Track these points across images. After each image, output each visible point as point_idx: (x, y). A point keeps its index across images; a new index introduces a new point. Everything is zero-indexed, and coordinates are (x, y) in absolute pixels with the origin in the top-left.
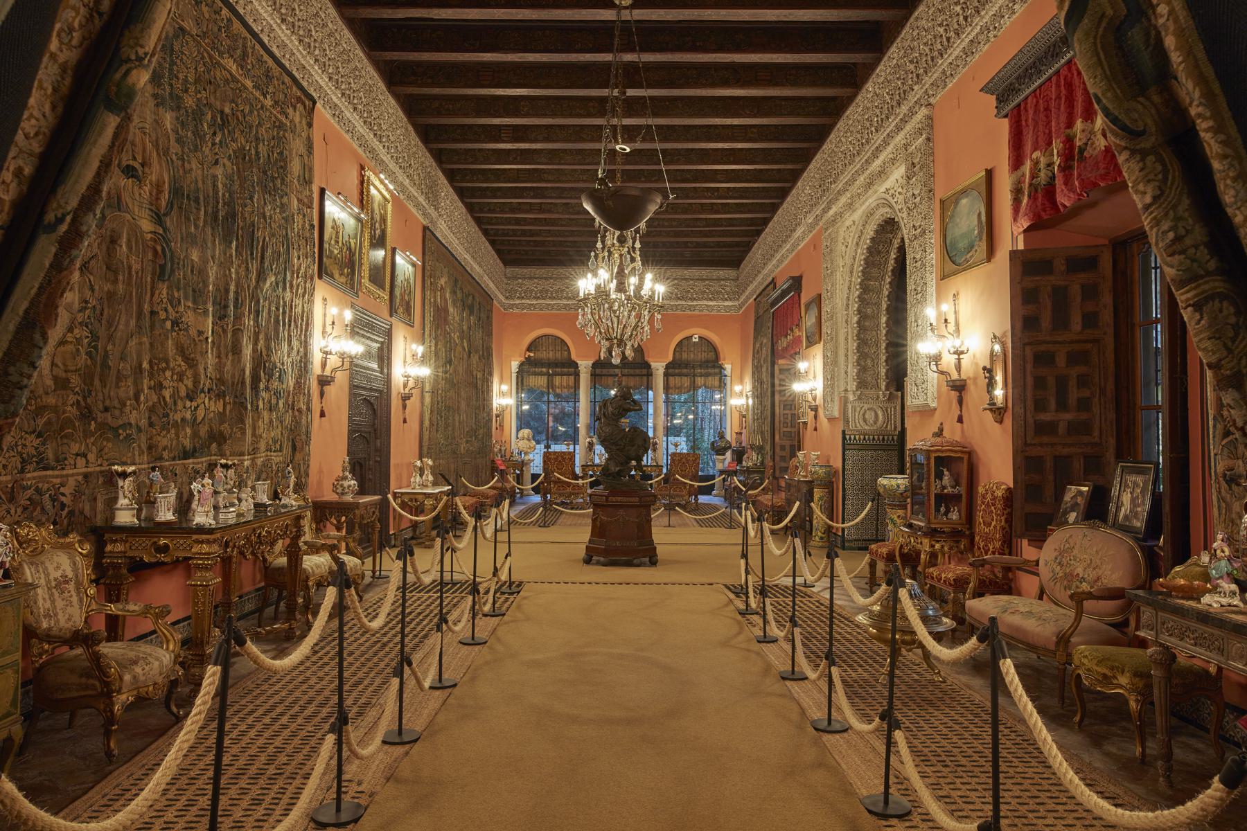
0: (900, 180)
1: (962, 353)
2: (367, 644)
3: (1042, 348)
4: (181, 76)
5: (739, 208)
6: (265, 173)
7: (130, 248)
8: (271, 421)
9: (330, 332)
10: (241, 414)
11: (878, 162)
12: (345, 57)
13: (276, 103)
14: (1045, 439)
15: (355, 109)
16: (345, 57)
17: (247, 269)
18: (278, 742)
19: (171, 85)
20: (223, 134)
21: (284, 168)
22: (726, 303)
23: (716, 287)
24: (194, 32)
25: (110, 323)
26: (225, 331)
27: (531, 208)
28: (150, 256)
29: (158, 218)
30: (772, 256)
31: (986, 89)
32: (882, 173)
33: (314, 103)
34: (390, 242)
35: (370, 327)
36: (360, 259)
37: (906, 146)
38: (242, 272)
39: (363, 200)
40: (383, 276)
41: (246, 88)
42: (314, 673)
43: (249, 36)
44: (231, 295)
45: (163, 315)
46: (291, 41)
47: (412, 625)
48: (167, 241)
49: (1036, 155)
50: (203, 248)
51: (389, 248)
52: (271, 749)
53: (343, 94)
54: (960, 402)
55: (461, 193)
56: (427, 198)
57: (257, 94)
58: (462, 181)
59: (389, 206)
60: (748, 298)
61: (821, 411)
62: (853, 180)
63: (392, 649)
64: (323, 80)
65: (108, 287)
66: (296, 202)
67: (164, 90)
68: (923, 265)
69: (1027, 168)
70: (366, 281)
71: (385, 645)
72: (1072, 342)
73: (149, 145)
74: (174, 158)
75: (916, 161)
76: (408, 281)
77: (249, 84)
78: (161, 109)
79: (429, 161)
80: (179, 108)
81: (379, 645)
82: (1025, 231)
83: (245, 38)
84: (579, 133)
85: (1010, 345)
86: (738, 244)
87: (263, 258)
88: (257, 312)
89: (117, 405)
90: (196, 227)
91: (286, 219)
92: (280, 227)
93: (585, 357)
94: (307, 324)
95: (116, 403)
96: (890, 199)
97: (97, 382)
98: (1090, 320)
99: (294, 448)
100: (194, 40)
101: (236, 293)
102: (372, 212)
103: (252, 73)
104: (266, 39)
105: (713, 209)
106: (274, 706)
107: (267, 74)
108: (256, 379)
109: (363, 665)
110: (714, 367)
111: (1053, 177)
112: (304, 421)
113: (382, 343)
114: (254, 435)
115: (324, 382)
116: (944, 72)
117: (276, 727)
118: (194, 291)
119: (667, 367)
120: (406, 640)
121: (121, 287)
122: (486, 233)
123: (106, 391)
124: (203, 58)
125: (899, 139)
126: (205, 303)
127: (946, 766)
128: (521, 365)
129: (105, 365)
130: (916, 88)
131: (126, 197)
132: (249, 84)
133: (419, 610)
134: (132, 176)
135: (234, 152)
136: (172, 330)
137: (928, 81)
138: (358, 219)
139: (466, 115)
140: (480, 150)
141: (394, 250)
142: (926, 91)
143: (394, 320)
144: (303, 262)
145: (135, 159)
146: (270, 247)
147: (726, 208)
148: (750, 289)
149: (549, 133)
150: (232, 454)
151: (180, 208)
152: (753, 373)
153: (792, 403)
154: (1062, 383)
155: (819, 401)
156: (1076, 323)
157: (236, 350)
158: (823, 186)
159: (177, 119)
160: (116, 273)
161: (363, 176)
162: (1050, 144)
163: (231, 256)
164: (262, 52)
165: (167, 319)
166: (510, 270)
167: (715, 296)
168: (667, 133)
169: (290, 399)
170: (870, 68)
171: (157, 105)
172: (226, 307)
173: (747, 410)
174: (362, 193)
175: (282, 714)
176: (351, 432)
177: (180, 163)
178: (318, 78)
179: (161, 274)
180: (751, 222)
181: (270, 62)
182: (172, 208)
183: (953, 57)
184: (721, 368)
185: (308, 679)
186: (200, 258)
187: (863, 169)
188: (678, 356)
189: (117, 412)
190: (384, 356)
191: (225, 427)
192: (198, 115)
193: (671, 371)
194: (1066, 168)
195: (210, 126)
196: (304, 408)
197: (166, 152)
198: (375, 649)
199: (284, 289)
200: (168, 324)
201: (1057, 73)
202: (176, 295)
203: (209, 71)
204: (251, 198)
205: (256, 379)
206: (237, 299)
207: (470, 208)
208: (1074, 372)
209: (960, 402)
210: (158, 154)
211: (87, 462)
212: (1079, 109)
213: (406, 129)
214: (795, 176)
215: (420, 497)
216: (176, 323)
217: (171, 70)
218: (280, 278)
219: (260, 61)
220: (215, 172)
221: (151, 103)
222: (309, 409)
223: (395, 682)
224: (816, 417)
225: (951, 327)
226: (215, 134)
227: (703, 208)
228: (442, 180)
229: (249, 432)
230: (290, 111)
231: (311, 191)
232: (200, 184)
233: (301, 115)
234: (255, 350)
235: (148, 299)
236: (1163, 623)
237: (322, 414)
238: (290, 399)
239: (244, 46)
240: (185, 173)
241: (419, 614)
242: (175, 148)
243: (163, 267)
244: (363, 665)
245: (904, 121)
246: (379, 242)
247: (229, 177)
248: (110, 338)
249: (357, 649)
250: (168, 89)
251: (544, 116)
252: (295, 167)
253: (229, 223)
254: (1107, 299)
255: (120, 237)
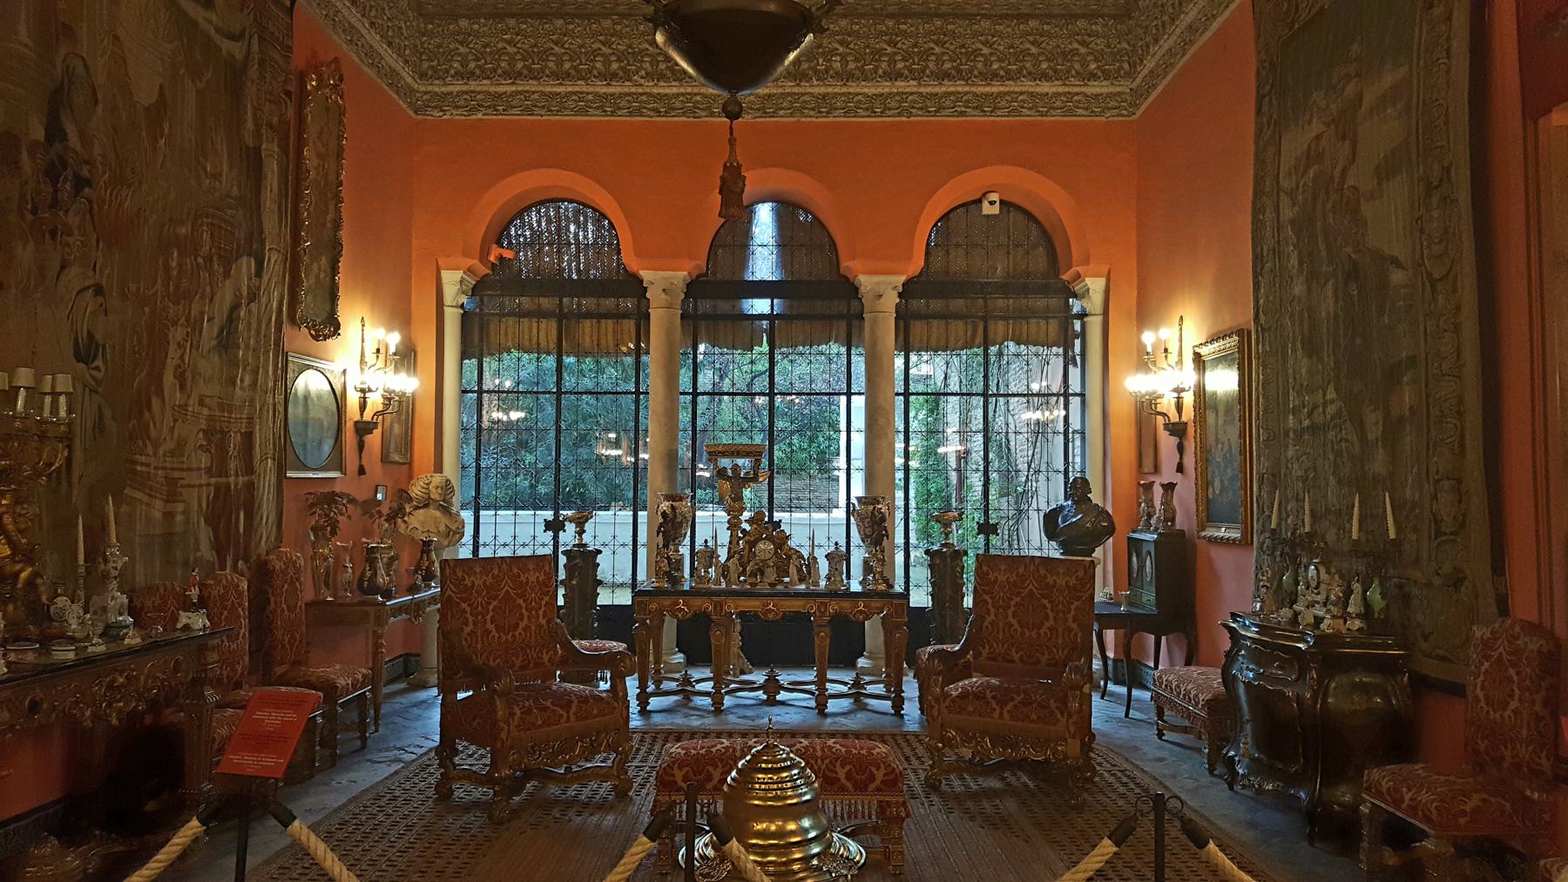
22: (1095, 88)
93: (660, 258)
110: (1044, 290)
115: (363, 429)
119: (907, 292)
188: (938, 263)
193: (919, 304)
225: (1173, 358)
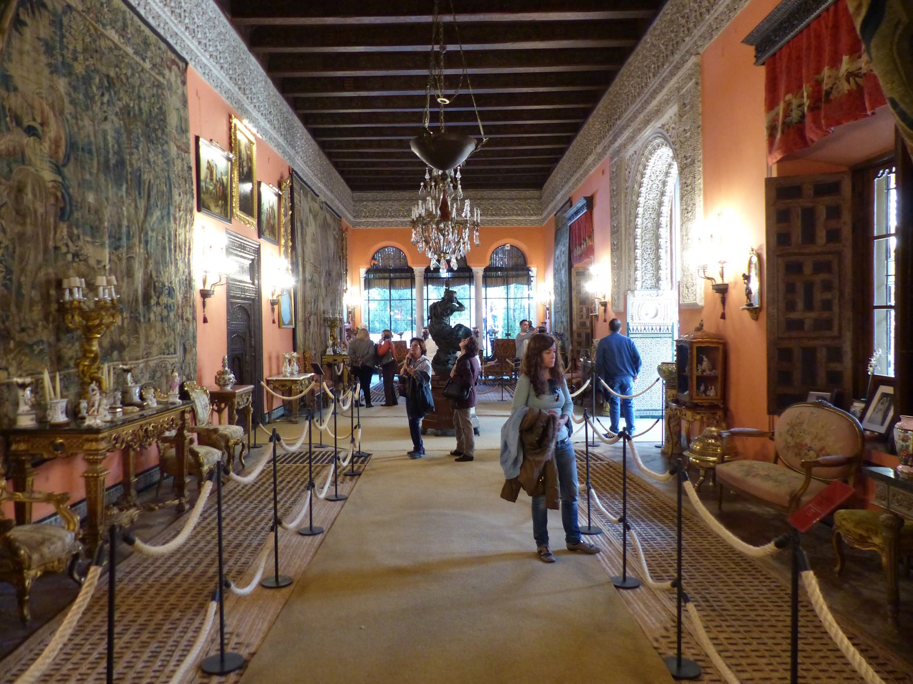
0: (673, 117)
1: (724, 262)
2: (247, 511)
3: (793, 258)
4: (71, 47)
5: (540, 141)
6: (147, 125)
7: (35, 195)
8: (163, 330)
9: (210, 255)
10: (136, 326)
11: (655, 103)
12: (211, 24)
13: (154, 65)
14: (794, 334)
15: (222, 67)
16: (211, 24)
17: (136, 207)
18: (173, 599)
19: (63, 55)
20: (110, 95)
21: (164, 120)
23: (523, 204)
24: (80, 8)
25: (22, 259)
26: (120, 259)
27: (370, 144)
28: (52, 201)
29: (58, 169)
30: (569, 179)
31: (747, 41)
32: (658, 112)
33: (187, 64)
34: (257, 176)
35: (242, 247)
36: (231, 192)
37: (679, 89)
38: (132, 211)
39: (232, 144)
40: (250, 205)
41: (127, 54)
42: (204, 537)
43: (128, 10)
44: (124, 230)
45: (64, 249)
46: (164, 12)
47: (283, 493)
48: (66, 188)
49: (789, 97)
50: (97, 191)
51: (255, 182)
52: (167, 606)
53: (211, 56)
54: (724, 301)
55: (315, 133)
56: (286, 139)
57: (138, 59)
58: (315, 123)
59: (254, 148)
60: (549, 214)
61: (609, 306)
62: (635, 116)
63: (267, 514)
64: (193, 45)
65: (18, 229)
66: (175, 148)
67: (56, 59)
68: (693, 189)
69: (781, 107)
70: (237, 211)
71: (261, 510)
72: (817, 254)
73: (47, 108)
74: (69, 117)
75: (687, 102)
76: (272, 208)
77: (130, 50)
78: (55, 77)
79: (286, 107)
80: (70, 74)
81: (257, 510)
82: (778, 162)
83: (124, 12)
84: (410, 83)
85: (765, 257)
86: (541, 170)
87: (149, 196)
88: (147, 242)
89: (32, 327)
90: (91, 174)
91: (167, 163)
92: (162, 170)
94: (190, 249)
95: (30, 325)
96: (665, 133)
97: (13, 308)
98: (834, 236)
99: (185, 350)
100: (81, 15)
101: (128, 227)
102: (240, 152)
103: (132, 41)
104: (142, 12)
105: (520, 142)
106: (170, 567)
107: (146, 43)
108: (147, 298)
109: (243, 529)
110: (523, 269)
111: (803, 116)
112: (191, 328)
113: (253, 260)
114: (147, 342)
116: (710, 26)
117: (172, 585)
118: (92, 228)
120: (279, 506)
121: (29, 229)
122: (336, 165)
123: (22, 315)
124: (89, 30)
125: (673, 83)
126: (102, 237)
127: (714, 610)
128: (368, 272)
129: (19, 294)
130: (687, 39)
131: (28, 152)
132: (130, 50)
133: (288, 479)
134: (34, 135)
135: (121, 109)
136: (73, 261)
137: (697, 33)
138: (229, 159)
139: (315, 70)
140: (327, 98)
141: (259, 183)
142: (695, 42)
143: (262, 241)
144: (183, 198)
145: (34, 120)
146: (155, 187)
147: (529, 141)
148: (551, 206)
149: (384, 83)
150: (130, 359)
151: (76, 159)
152: (555, 275)
153: (586, 303)
154: (809, 288)
155: (608, 299)
156: (821, 236)
157: (130, 274)
158: (610, 121)
159: (69, 84)
160: (24, 216)
161: (230, 123)
162: (801, 87)
163: (122, 197)
164: (140, 23)
165: (68, 252)
166: (357, 194)
167: (523, 212)
168: (479, 80)
169: (180, 311)
170: (648, 22)
171: (52, 73)
172: (120, 239)
173: (550, 304)
174: (230, 137)
175: (177, 574)
176: (230, 333)
177: (74, 121)
178: (189, 43)
179: (63, 214)
180: (552, 151)
181: (147, 31)
182: (69, 159)
183: (718, 12)
184: (529, 270)
185: (198, 542)
186: (96, 200)
187: (643, 107)
189: (31, 332)
190: (254, 268)
191: (124, 338)
192: (87, 80)
194: (814, 108)
195: (98, 88)
196: (190, 317)
197: (62, 112)
198: (254, 514)
199: (169, 220)
200: (69, 257)
201: (808, 26)
202: (75, 232)
203: (95, 41)
204: (137, 147)
205: (147, 298)
206: (129, 232)
207: (323, 146)
208: (819, 278)
209: (724, 301)
210: (55, 115)
211: (9, 374)
212: (826, 57)
213: (266, 82)
214: (585, 114)
215: (288, 383)
216: (76, 255)
217: (61, 42)
218: (165, 213)
219: (139, 31)
220: (102, 127)
221: (46, 71)
222: (194, 318)
223: (273, 534)
224: (605, 311)
226: (103, 95)
227: (512, 142)
228: (298, 123)
229: (142, 340)
230: (166, 72)
231: (188, 138)
232: (92, 138)
233: (176, 76)
234: (145, 273)
235: (52, 236)
236: (894, 496)
237: (205, 321)
238: (180, 311)
239: (124, 19)
240: (79, 129)
241: (289, 482)
242: (69, 108)
243: (63, 210)
244: (243, 529)
245: (677, 68)
246: (247, 176)
247: (117, 132)
248: (23, 271)
249: (238, 515)
250: (60, 59)
251: (380, 68)
252: (173, 120)
253: (117, 169)
254: (847, 217)
255: (25, 186)
